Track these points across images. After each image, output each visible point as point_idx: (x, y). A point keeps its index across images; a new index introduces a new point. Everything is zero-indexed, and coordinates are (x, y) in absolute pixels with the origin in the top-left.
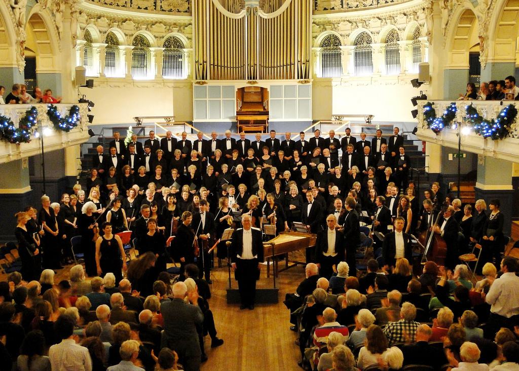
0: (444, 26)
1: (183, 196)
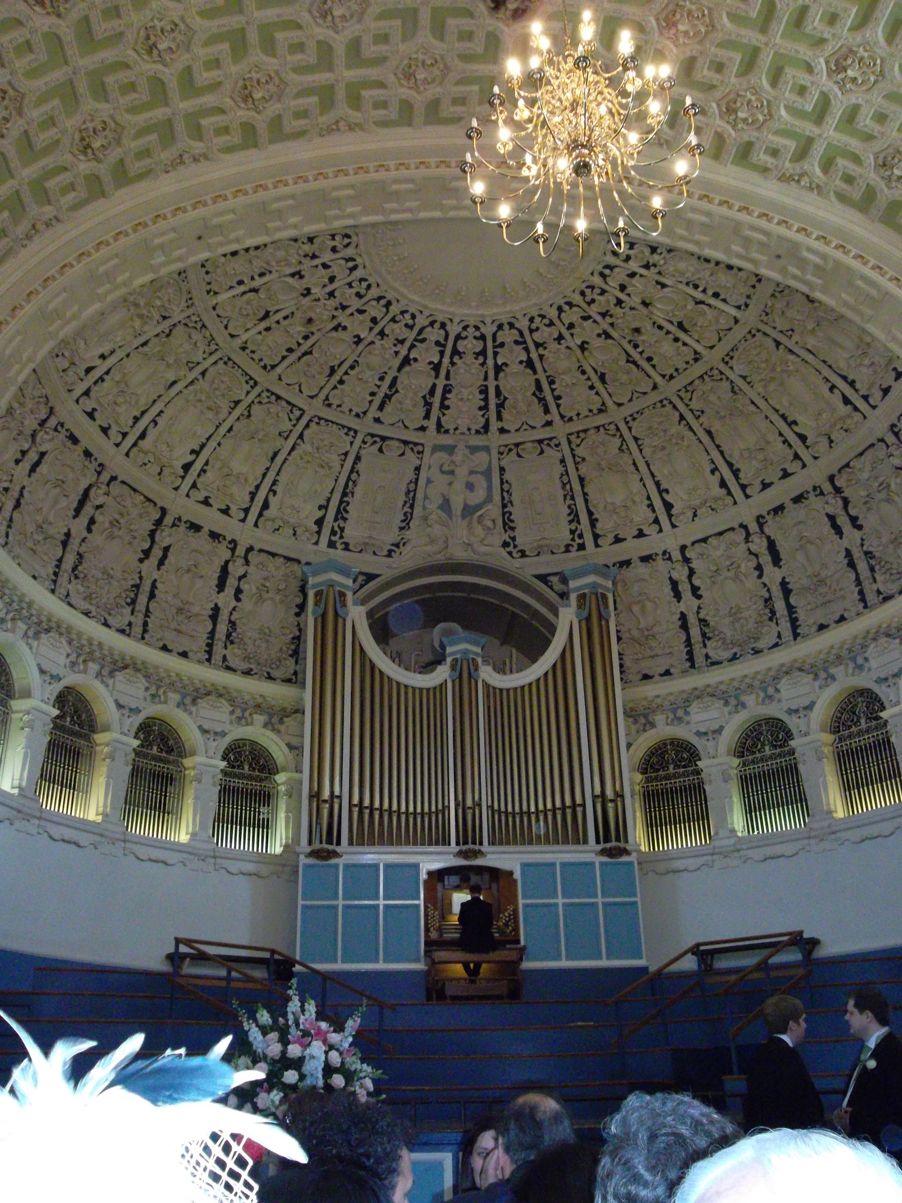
1: (265, 1012)
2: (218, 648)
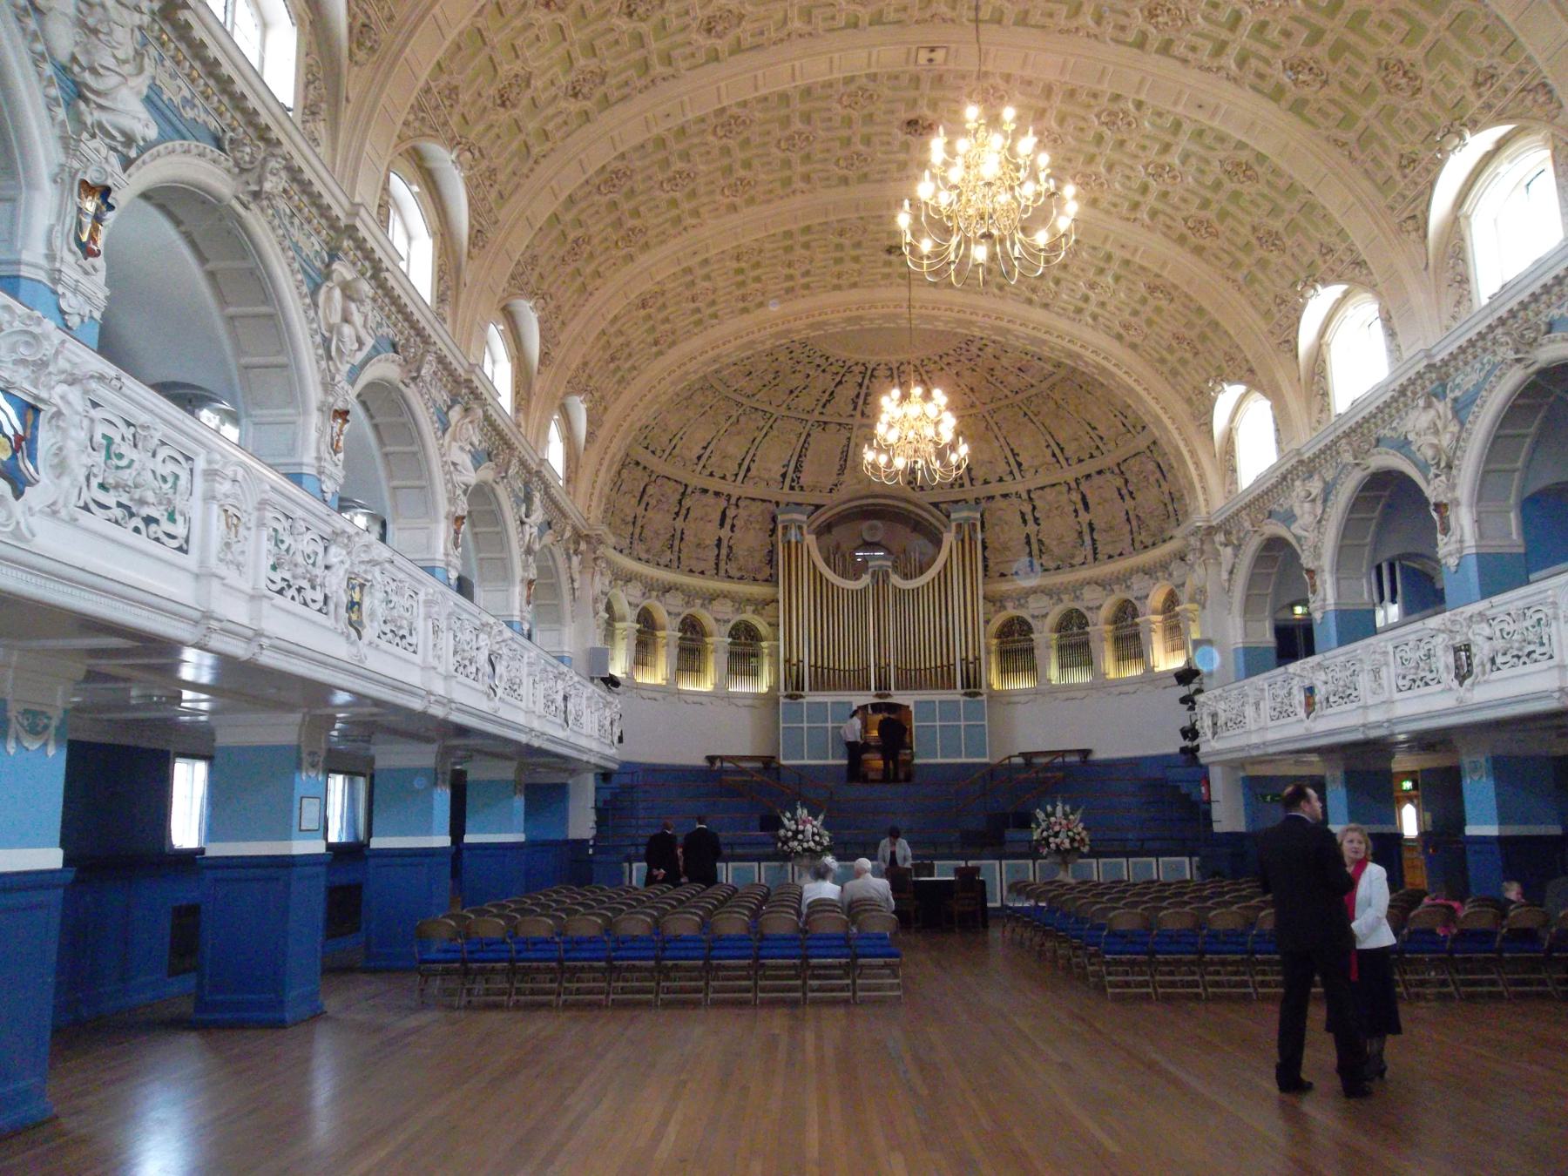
0: (1225, 576)
2: (722, 564)
